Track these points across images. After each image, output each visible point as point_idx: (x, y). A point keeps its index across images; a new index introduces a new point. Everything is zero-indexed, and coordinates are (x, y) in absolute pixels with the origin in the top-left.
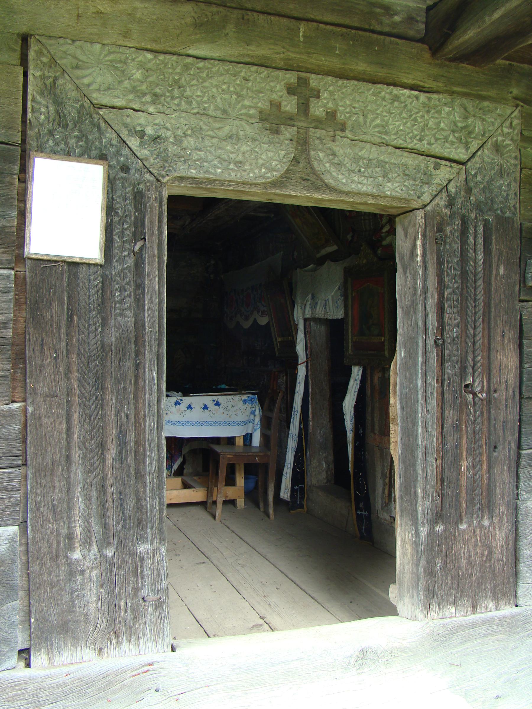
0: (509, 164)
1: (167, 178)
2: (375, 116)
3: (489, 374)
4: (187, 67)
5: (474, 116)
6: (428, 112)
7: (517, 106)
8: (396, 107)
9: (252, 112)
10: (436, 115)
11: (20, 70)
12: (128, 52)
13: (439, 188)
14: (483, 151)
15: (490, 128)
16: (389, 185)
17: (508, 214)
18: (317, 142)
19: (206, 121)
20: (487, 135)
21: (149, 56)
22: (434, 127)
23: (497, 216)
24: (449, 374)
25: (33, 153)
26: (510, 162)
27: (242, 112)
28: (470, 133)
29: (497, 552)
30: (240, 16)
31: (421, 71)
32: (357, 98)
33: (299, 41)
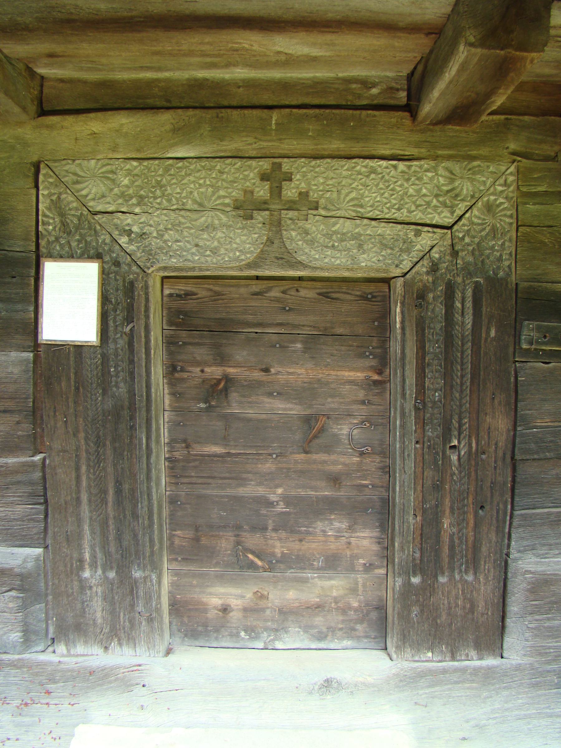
0: (502, 223)
1: (152, 269)
2: (350, 190)
3: (478, 435)
4: (167, 169)
5: (461, 178)
6: (408, 180)
7: (514, 162)
8: (373, 179)
9: (227, 201)
10: (417, 182)
11: (34, 191)
12: (117, 163)
13: (421, 254)
14: (472, 212)
15: (482, 188)
16: (365, 256)
17: (501, 274)
18: (289, 222)
19: (185, 215)
20: (477, 195)
21: (135, 163)
22: (414, 194)
23: (488, 279)
24: (429, 436)
25: (42, 260)
26: (505, 220)
27: (217, 202)
28: (457, 195)
29: (480, 606)
30: (215, 115)
31: (400, 140)
32: (332, 175)
33: (271, 129)
